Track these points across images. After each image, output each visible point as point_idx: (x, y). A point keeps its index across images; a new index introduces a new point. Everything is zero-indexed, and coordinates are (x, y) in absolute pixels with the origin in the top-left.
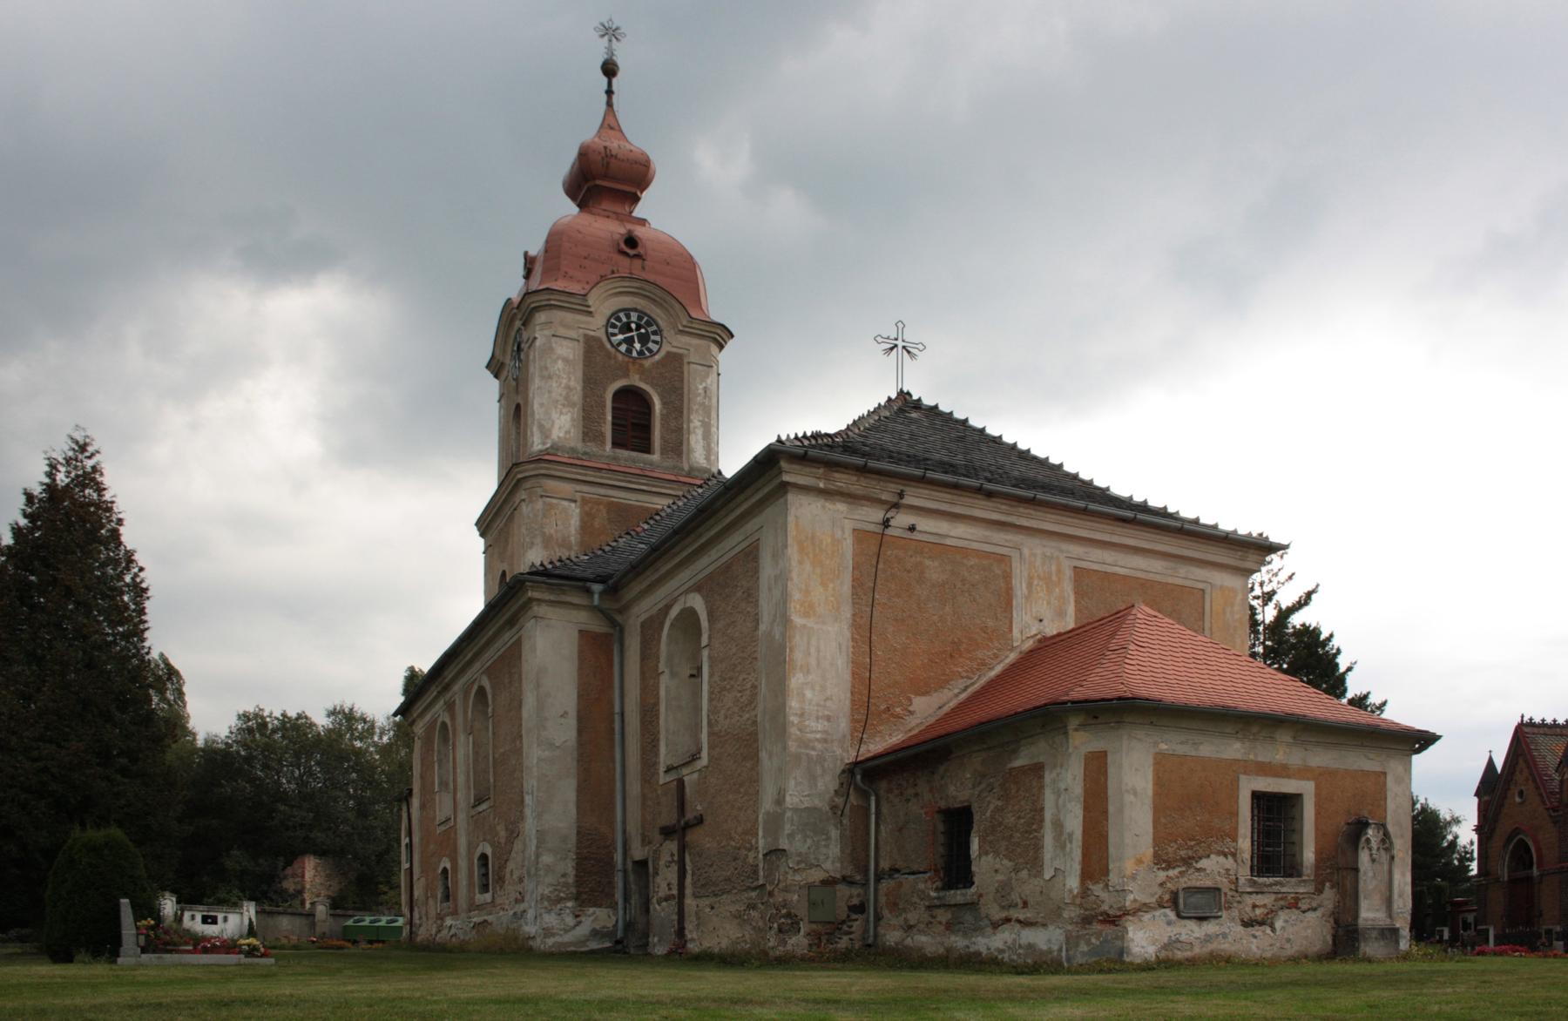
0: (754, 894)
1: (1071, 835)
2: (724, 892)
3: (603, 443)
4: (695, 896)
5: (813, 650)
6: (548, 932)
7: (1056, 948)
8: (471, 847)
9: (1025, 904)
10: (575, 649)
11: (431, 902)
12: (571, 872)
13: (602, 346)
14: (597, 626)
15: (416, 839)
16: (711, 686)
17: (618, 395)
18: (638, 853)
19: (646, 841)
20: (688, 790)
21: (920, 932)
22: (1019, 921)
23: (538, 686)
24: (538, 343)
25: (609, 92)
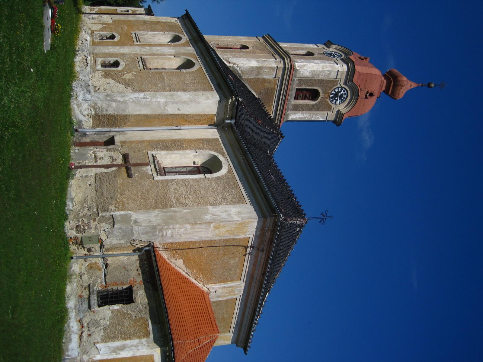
0: (95, 210)
1: (119, 354)
2: (97, 192)
3: (298, 86)
4: (96, 174)
5: (200, 230)
6: (79, 105)
7: (69, 353)
8: (123, 55)
9: (90, 335)
10: (208, 113)
12: (109, 113)
13: (334, 86)
15: (131, 18)
18: (117, 139)
19: (123, 143)
22: (82, 333)
23: (191, 101)
24: (336, 65)
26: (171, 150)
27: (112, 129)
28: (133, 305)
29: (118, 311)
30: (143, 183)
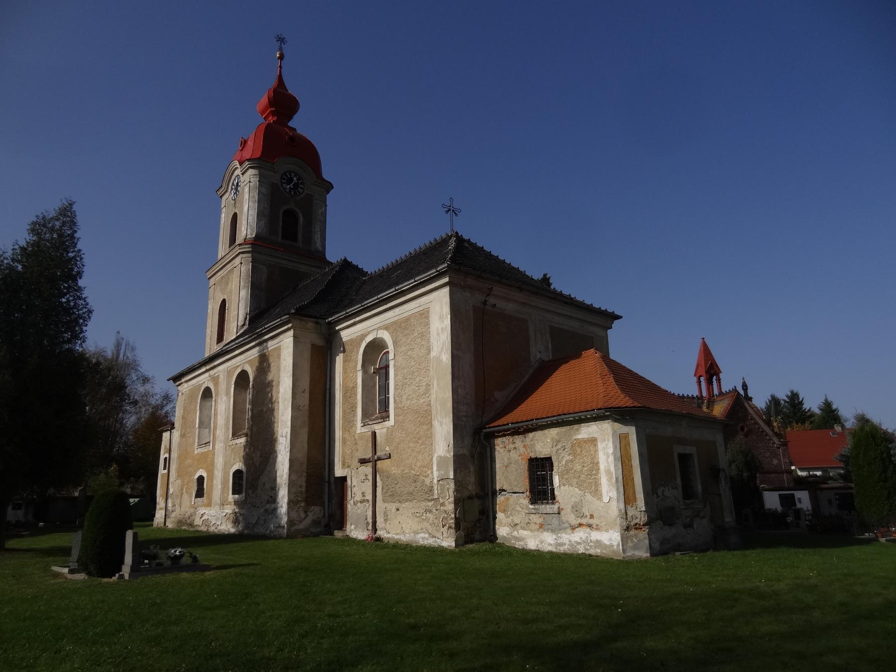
0: (430, 504)
2: (407, 500)
7: (615, 544)
11: (185, 496)
12: (304, 484)
14: (320, 342)
15: (174, 455)
16: (395, 381)
17: (285, 211)
20: (378, 438)
21: (523, 529)
25: (281, 67)
27: (327, 479)
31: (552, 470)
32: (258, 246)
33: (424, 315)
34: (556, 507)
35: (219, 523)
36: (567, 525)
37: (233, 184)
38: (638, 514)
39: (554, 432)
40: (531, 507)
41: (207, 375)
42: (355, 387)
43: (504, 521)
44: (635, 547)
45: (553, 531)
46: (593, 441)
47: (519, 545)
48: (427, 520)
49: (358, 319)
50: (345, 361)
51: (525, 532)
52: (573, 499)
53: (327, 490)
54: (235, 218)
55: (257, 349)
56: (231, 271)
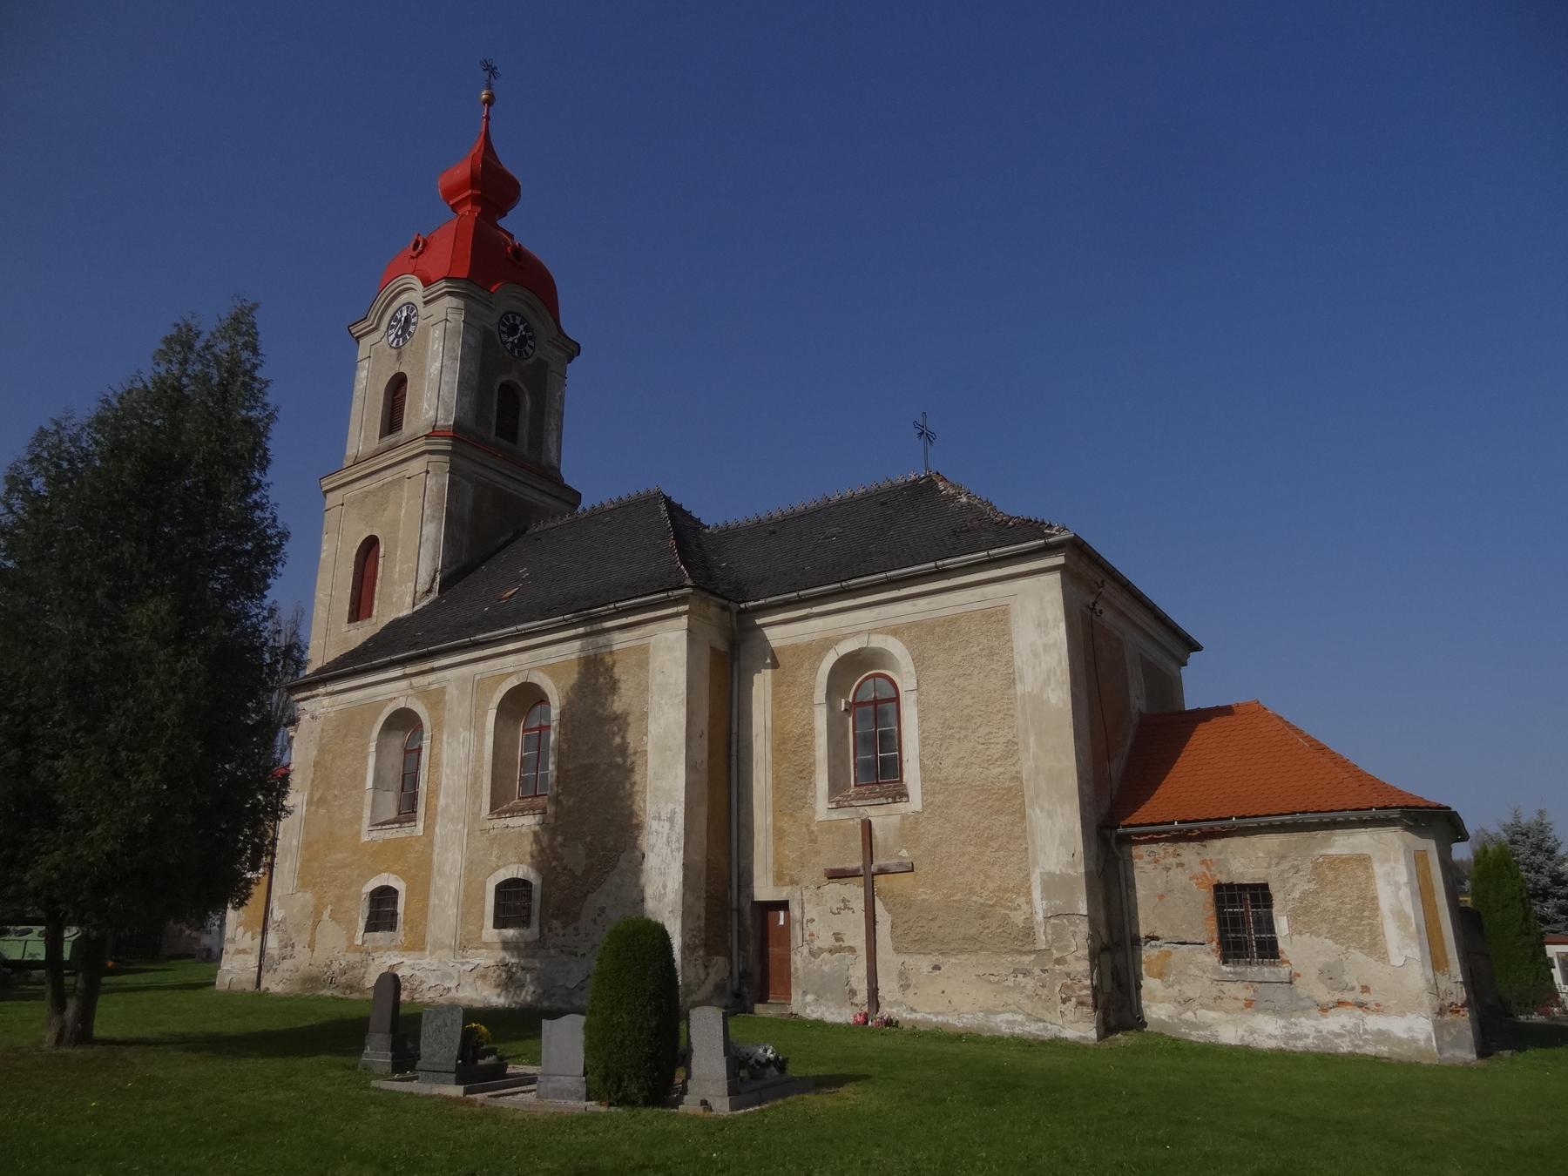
0: (1027, 959)
7: (1422, 1037)
21: (1207, 1007)
25: (488, 118)
26: (814, 763)
27: (735, 905)
28: (1273, 888)
29: (1294, 917)
30: (931, 839)
31: (1270, 906)
32: (462, 440)
33: (998, 619)
34: (1284, 971)
35: (452, 985)
36: (1308, 1003)
37: (394, 318)
38: (1452, 987)
39: (1273, 841)
40: (1224, 968)
41: (404, 684)
42: (808, 734)
43: (1159, 994)
44: (1456, 1044)
45: (1277, 1012)
46: (1363, 861)
47: (1196, 1036)
48: (1020, 989)
49: (816, 610)
50: (776, 685)
51: (1212, 1014)
52: (1322, 959)
53: (735, 926)
54: (398, 385)
55: (577, 644)
56: (397, 483)
